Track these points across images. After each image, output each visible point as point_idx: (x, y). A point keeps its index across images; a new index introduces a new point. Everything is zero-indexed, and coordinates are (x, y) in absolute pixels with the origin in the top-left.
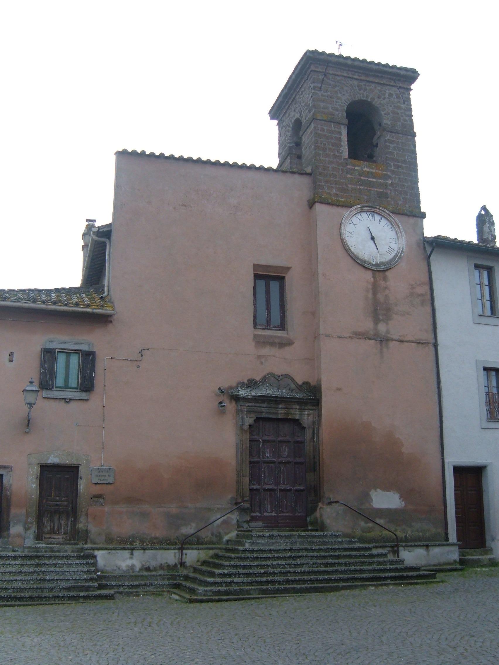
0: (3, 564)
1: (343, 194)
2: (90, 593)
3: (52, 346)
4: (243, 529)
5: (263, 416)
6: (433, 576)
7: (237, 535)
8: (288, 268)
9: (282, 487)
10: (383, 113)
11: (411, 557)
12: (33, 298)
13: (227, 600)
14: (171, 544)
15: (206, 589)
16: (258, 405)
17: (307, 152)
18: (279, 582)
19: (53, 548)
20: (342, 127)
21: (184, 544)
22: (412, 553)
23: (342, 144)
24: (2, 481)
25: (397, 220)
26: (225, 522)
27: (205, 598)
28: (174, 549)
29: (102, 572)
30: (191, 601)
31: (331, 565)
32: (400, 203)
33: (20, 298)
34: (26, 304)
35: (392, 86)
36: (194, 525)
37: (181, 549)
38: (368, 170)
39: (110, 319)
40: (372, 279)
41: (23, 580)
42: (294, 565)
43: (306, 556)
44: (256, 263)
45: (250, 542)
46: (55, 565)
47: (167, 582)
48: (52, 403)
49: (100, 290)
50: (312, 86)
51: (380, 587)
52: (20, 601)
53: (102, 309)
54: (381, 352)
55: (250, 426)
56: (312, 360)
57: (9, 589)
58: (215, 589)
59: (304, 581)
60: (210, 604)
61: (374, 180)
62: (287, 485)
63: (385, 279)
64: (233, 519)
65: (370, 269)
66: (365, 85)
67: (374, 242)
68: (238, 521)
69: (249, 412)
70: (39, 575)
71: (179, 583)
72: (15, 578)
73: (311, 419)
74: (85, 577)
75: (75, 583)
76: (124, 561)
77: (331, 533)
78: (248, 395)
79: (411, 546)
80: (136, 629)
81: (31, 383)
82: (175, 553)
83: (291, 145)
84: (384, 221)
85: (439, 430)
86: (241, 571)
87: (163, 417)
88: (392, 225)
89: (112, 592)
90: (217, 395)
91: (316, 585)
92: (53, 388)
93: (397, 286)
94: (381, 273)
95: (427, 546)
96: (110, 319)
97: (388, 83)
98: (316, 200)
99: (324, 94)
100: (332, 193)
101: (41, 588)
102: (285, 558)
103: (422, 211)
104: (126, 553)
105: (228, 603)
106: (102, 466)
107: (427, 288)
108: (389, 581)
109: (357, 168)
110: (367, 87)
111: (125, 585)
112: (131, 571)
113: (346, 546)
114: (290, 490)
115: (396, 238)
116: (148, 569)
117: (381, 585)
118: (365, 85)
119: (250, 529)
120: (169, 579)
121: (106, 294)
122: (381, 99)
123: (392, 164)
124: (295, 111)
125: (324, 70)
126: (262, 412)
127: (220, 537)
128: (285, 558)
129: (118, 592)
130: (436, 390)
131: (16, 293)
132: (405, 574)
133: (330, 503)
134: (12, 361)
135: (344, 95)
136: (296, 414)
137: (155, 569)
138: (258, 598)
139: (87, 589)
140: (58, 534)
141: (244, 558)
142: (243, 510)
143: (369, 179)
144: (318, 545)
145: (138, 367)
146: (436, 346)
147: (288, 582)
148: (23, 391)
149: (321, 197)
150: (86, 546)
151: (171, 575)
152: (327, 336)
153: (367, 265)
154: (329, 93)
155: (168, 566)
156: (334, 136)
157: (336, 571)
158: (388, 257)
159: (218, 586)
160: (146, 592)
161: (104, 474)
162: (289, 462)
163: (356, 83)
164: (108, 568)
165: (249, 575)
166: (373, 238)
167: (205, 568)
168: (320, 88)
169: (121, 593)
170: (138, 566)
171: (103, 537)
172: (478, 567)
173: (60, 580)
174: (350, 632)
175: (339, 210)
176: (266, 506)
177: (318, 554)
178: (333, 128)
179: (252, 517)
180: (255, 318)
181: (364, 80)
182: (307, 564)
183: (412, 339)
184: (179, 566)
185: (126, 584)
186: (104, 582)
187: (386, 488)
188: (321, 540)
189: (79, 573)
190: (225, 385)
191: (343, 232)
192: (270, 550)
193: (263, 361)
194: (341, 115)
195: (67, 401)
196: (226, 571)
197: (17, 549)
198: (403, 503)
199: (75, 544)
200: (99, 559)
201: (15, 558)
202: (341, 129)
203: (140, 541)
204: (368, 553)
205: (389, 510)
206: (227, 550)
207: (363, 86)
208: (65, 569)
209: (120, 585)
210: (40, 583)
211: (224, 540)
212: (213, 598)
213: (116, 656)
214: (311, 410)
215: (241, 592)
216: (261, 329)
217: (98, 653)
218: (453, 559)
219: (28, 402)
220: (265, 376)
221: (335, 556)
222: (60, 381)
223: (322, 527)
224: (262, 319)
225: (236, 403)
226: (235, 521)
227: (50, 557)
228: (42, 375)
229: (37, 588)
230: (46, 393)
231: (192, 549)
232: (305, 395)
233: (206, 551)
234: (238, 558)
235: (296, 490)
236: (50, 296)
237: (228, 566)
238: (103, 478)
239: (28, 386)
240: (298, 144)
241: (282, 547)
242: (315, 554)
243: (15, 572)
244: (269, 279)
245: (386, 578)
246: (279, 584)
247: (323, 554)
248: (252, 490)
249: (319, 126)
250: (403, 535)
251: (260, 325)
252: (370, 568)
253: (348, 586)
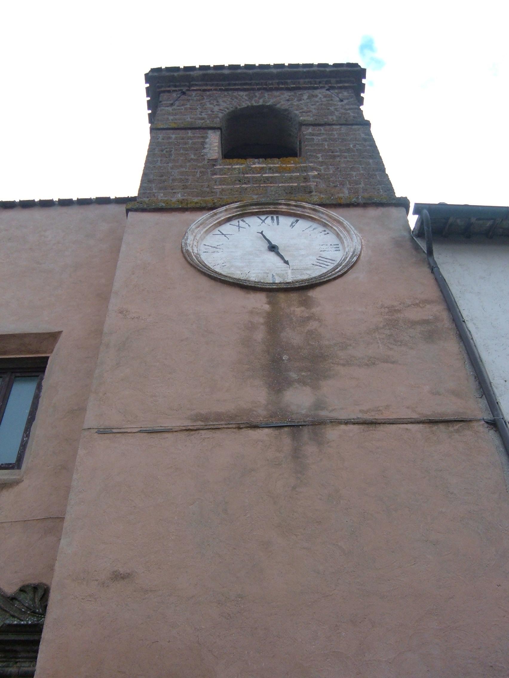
54: (296, 454)
67: (282, 257)
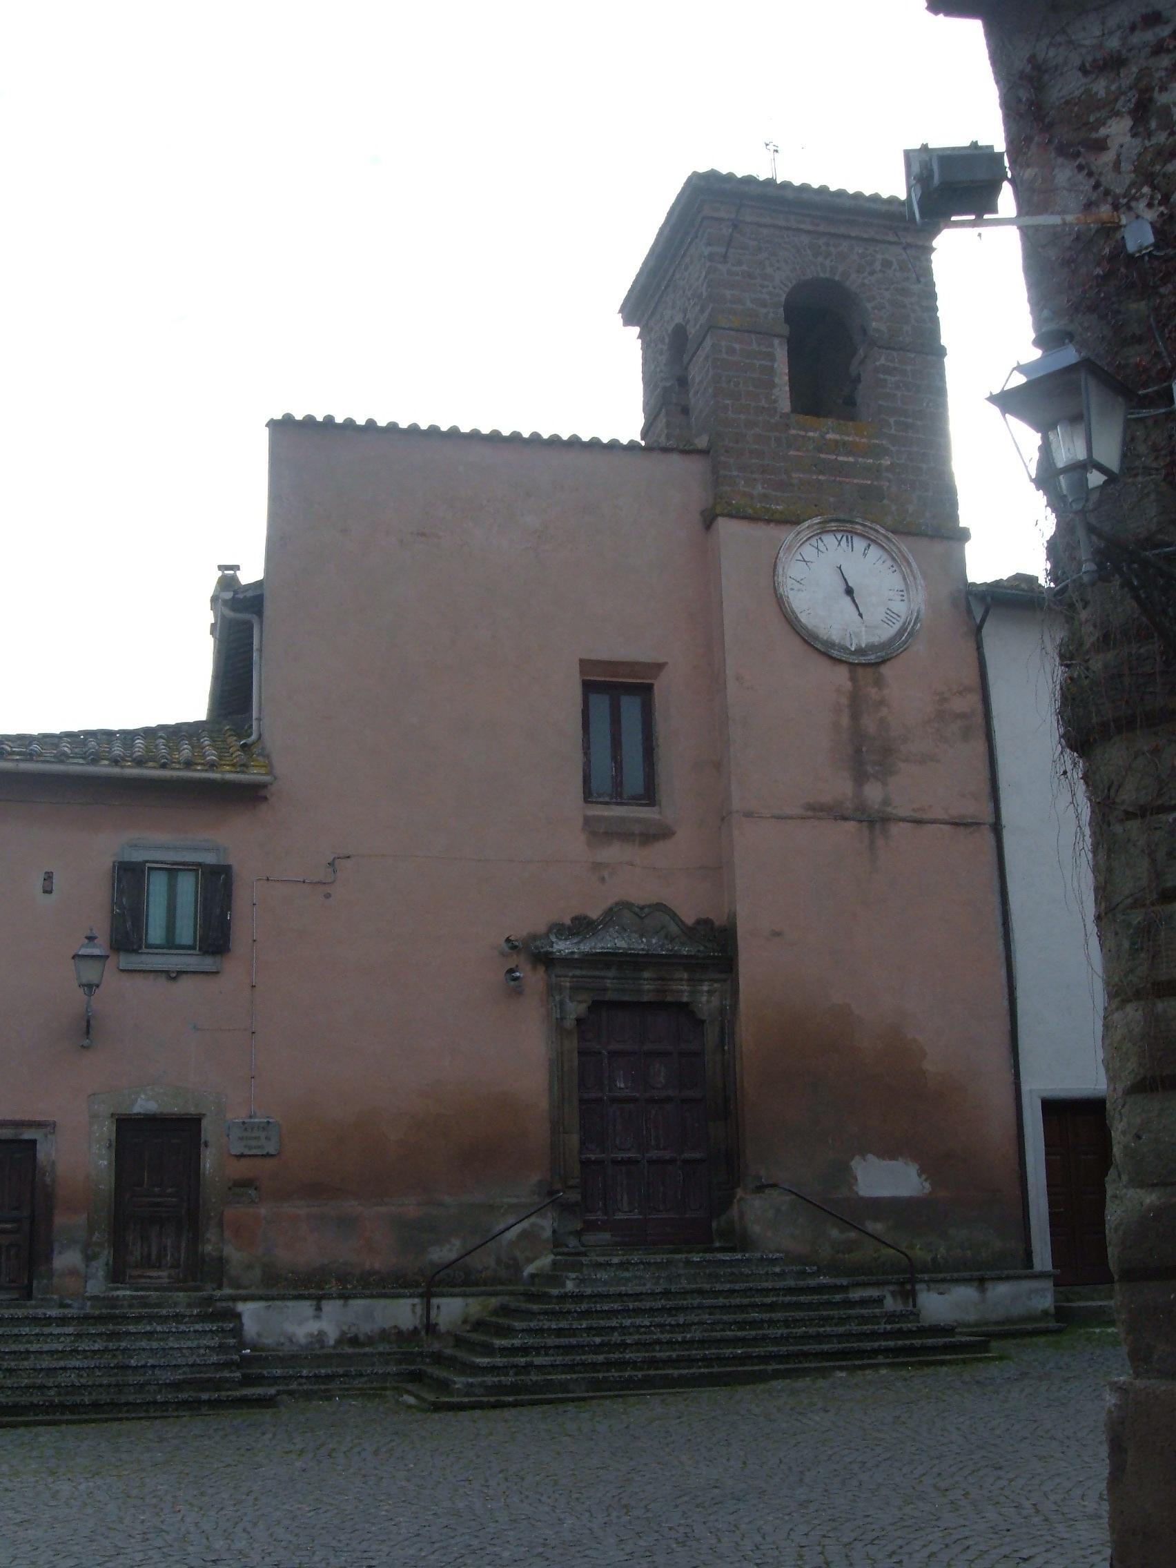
0: (37, 1335)
1: (779, 494)
2: (223, 1393)
3: (137, 856)
4: (566, 1250)
5: (607, 998)
6: (983, 1346)
7: (554, 1263)
8: (659, 667)
9: (654, 1154)
10: (869, 306)
11: (941, 1304)
12: (92, 753)
13: (515, 1405)
14: (406, 1285)
15: (470, 1380)
16: (597, 973)
17: (699, 401)
18: (634, 1364)
19: (147, 1297)
20: (776, 342)
21: (431, 1284)
22: (946, 1296)
23: (777, 380)
24: (35, 1155)
25: (904, 548)
26: (526, 1233)
27: (466, 1400)
28: (411, 1296)
29: (254, 1348)
30: (437, 1407)
31: (753, 1324)
32: (911, 508)
33: (64, 754)
34: (77, 767)
35: (890, 243)
36: (457, 1243)
37: (427, 1296)
38: (837, 437)
39: (263, 793)
40: (849, 683)
41: (79, 1369)
42: (670, 1325)
43: (700, 1307)
44: (586, 657)
45: (577, 1278)
46: (150, 1335)
47: (393, 1369)
48: (139, 980)
49: (242, 730)
50: (706, 251)
51: (860, 1372)
52: (73, 1413)
53: (243, 772)
55: (579, 1021)
56: (717, 870)
57: (49, 1388)
58: (490, 1379)
59: (691, 1361)
60: (478, 1413)
61: (851, 459)
62: (664, 1149)
63: (879, 682)
64: (542, 1228)
65: (846, 662)
66: (827, 245)
67: (854, 601)
68: (554, 1232)
69: (575, 989)
70: (114, 1356)
71: (420, 1375)
72: (62, 1364)
73: (715, 1001)
74: (214, 1359)
75: (192, 1373)
76: (304, 1324)
77: (758, 1255)
78: (573, 953)
79: (943, 1281)
80: (298, 1464)
81: (91, 939)
82: (414, 1305)
83: (668, 384)
84: (874, 552)
85: (1008, 1018)
86: (551, 1341)
87: (389, 1005)
88: (894, 559)
89: (272, 1391)
90: (503, 954)
91: (716, 1370)
92: (140, 947)
93: (907, 697)
94: (869, 670)
95: (981, 1282)
96: (263, 793)
97: (878, 237)
98: (718, 511)
99: (734, 269)
100: (755, 493)
101: (117, 1385)
102: (651, 1311)
103: (961, 525)
104: (306, 1307)
105: (514, 1411)
106: (251, 1117)
107: (974, 699)
108: (881, 1359)
109: (811, 434)
110: (832, 249)
111: (301, 1377)
112: (317, 1346)
113: (791, 1283)
114: (672, 1161)
115: (903, 587)
116: (354, 1341)
117: (862, 1368)
118: (827, 245)
119: (583, 1249)
120: (399, 1362)
121: (254, 737)
122: (866, 274)
123: (892, 420)
124: (673, 307)
125: (733, 216)
126: (605, 990)
127: (516, 1267)
128: (651, 1311)
129: (286, 1392)
130: (1000, 929)
131: (56, 741)
132: (917, 1342)
133: (760, 1189)
134: (51, 892)
135: (778, 269)
136: (682, 991)
137: (370, 1341)
138: (583, 1399)
139: (218, 1385)
140: (159, 1267)
141: (561, 1312)
142: (566, 1208)
143: (841, 458)
144: (730, 1282)
145: (328, 896)
146: (997, 828)
147: (653, 1363)
148: (73, 957)
149: (730, 504)
150: (218, 1293)
151: (403, 1353)
152: (748, 815)
153: (835, 653)
154: (744, 267)
155: (400, 1333)
156: (757, 363)
157: (764, 1338)
158: (886, 633)
159: (498, 1375)
160: (347, 1390)
161: (256, 1134)
162: (669, 1100)
163: (806, 239)
164: (268, 1341)
165: (568, 1349)
166: (849, 591)
167: (475, 1337)
168: (725, 256)
169: (291, 1393)
170: (332, 1335)
171: (257, 1272)
172: (1097, 1327)
173: (160, 1366)
174: (744, 1463)
175: (772, 530)
176: (619, 1198)
177: (726, 1302)
178: (755, 347)
179: (585, 1222)
180: (587, 779)
181: (824, 234)
182: (701, 1323)
183: (942, 815)
184: (423, 1333)
185: (305, 1373)
186: (254, 1371)
187: (889, 1152)
188: (735, 1270)
189: (202, 1351)
190: (520, 931)
191: (780, 579)
192: (620, 1295)
193: (606, 874)
194: (774, 316)
195: (173, 976)
196: (517, 1342)
197: (69, 1302)
198: (927, 1185)
199: (197, 1289)
200: (246, 1320)
201: (63, 1321)
202: (772, 345)
203: (339, 1279)
204: (838, 1297)
205: (894, 1202)
206: (531, 1297)
207: (823, 248)
208: (172, 1343)
209: (291, 1377)
210: (116, 1375)
211: (525, 1274)
212: (485, 1399)
213: (239, 1514)
214: (715, 981)
215: (549, 1386)
216: (601, 803)
217: (201, 1509)
218: (1040, 1307)
219: (84, 981)
220: (611, 909)
221: (764, 1305)
222: (156, 933)
223: (739, 1240)
224: (602, 780)
225: (546, 971)
226: (548, 1233)
227: (139, 1319)
228: (117, 921)
229: (109, 1386)
230: (125, 961)
231: (453, 1295)
232: (702, 948)
233: (481, 1299)
234: (545, 1313)
235: (685, 1162)
236: (133, 746)
237: (523, 1331)
238: (254, 1143)
239: (83, 946)
240: (683, 382)
241: (648, 1288)
242: (721, 1301)
243: (62, 1352)
244: (617, 695)
245: (875, 1352)
246: (634, 1369)
247: (737, 1301)
248: (585, 1163)
249: (723, 343)
250: (929, 1258)
251: (600, 795)
252: (841, 1329)
253: (786, 1370)
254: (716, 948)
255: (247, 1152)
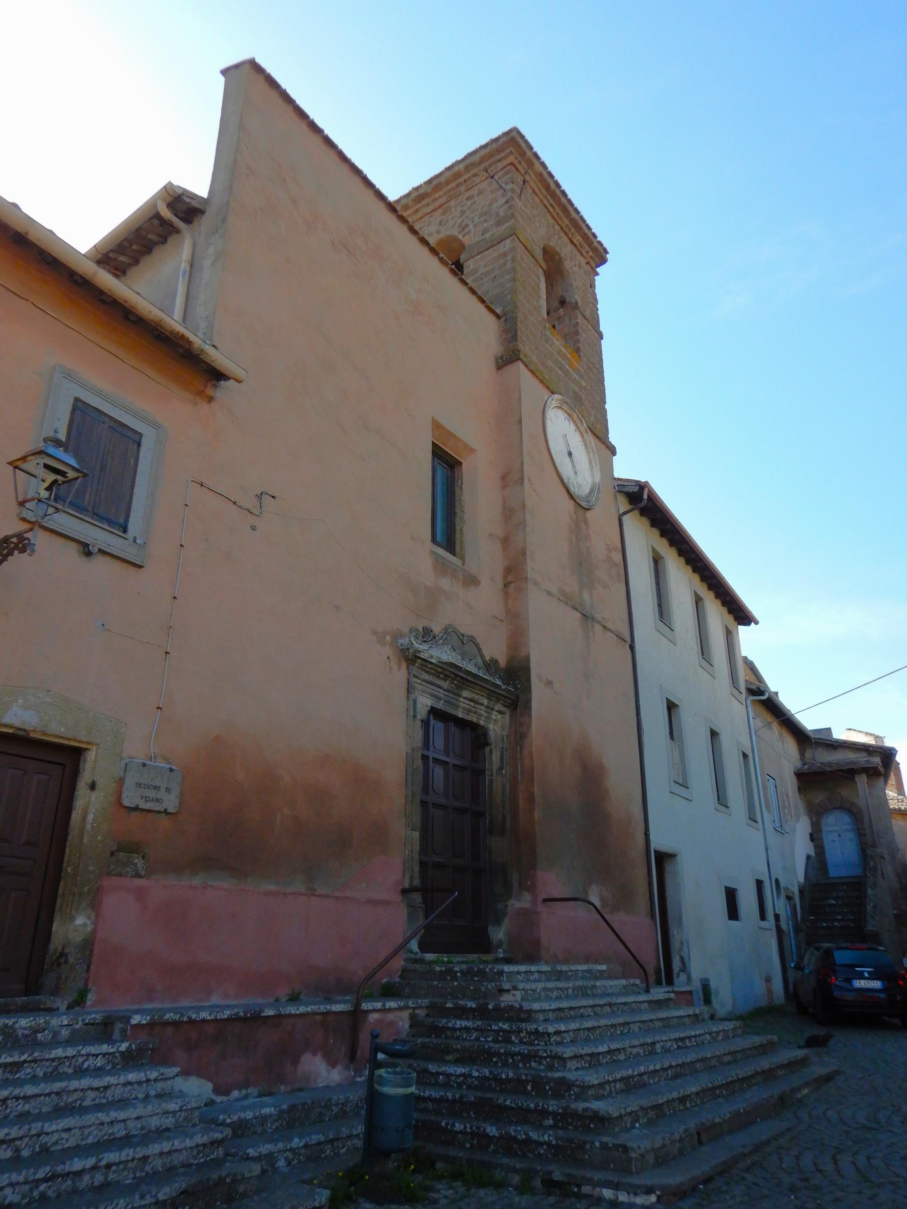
9: (437, 859)
238: (152, 794)
254: (512, 683)
255: (143, 805)
